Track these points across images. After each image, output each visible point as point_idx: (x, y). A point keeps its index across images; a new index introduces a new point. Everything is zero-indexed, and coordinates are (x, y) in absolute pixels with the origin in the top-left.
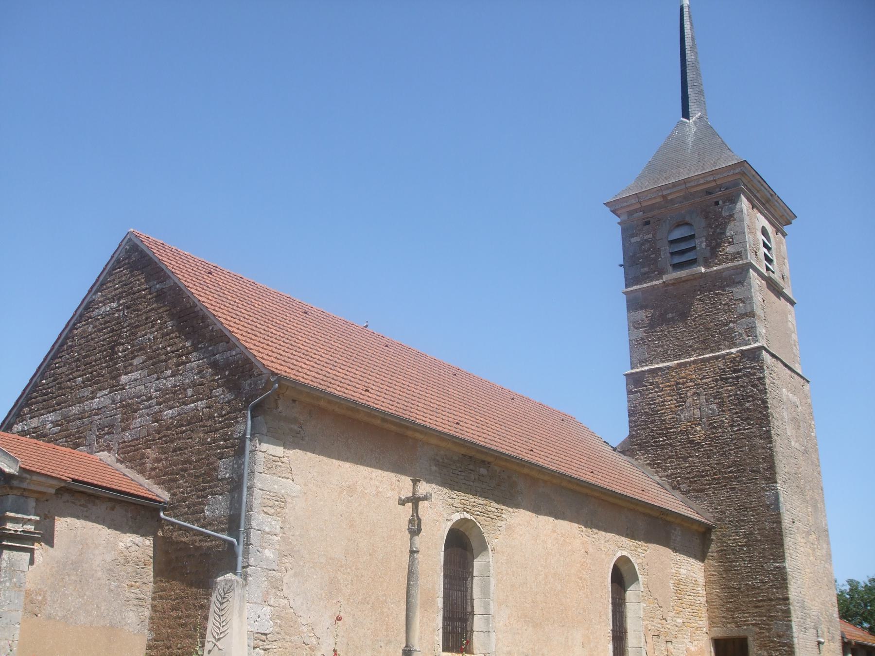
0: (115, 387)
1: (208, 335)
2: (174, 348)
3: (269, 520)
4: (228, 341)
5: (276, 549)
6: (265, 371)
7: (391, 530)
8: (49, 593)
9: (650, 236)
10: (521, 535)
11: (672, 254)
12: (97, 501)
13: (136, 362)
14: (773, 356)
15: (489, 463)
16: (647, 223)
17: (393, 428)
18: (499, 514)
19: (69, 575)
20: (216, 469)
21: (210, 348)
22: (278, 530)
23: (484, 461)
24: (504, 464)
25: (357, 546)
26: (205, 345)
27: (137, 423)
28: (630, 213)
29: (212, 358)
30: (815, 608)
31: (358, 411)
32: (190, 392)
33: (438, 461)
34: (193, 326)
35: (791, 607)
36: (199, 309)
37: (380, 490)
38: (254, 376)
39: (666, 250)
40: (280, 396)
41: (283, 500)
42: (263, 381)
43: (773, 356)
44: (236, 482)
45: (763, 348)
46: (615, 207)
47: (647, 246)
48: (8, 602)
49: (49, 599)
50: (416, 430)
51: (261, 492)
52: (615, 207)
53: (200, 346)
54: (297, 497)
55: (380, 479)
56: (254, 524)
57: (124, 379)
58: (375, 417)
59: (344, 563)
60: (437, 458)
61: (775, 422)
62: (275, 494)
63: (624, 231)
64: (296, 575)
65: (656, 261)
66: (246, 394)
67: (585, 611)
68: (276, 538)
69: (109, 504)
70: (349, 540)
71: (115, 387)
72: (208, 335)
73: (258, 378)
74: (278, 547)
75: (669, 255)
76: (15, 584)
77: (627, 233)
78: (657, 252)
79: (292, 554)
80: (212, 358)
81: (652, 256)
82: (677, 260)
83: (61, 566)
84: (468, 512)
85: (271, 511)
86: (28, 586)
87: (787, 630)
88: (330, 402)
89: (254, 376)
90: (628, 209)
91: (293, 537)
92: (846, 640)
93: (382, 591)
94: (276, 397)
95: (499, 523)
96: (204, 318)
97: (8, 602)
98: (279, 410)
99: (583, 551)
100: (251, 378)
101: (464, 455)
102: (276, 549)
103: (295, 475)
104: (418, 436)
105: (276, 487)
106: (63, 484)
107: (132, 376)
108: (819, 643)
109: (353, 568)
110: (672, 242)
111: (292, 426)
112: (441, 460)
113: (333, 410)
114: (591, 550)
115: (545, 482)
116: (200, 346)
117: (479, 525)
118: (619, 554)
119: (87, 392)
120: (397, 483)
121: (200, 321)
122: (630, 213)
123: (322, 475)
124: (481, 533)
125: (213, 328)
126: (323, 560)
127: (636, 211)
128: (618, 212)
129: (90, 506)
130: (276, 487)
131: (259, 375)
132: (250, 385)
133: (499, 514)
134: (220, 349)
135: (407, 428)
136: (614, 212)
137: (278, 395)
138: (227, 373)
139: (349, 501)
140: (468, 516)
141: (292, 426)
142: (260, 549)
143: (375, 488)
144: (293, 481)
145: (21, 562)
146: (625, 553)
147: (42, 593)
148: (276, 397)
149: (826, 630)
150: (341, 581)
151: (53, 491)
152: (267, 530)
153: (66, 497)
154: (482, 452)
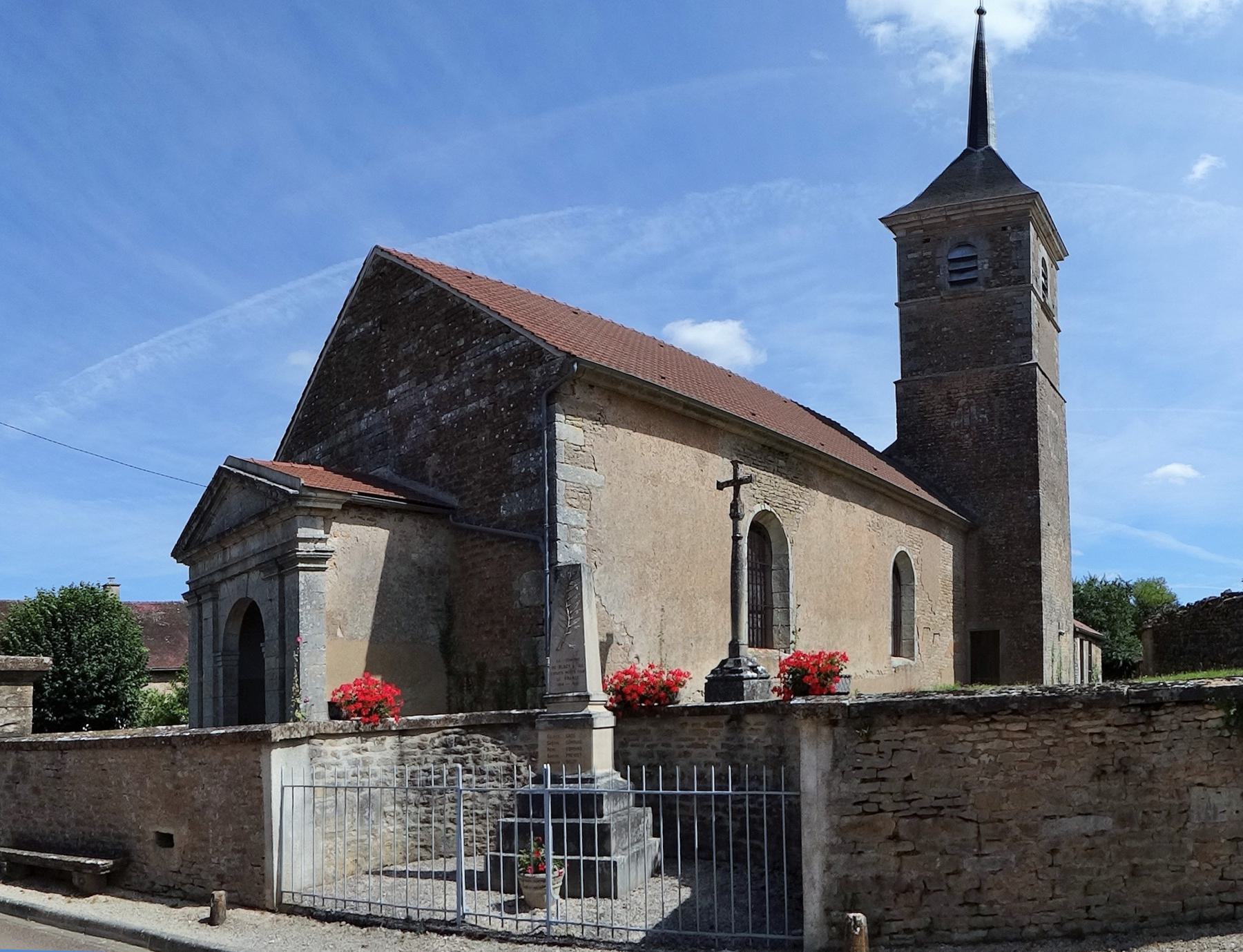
0: (382, 403)
1: (482, 330)
2: (445, 351)
3: (576, 512)
4: (507, 330)
5: (584, 544)
6: (558, 355)
7: (696, 522)
8: (349, 613)
9: (930, 253)
10: (816, 528)
11: (951, 272)
12: (385, 513)
13: (402, 374)
14: (1043, 373)
15: (787, 454)
16: (927, 241)
17: (696, 415)
18: (797, 507)
19: (366, 592)
20: (510, 465)
21: (487, 343)
22: (585, 524)
23: (782, 453)
24: (801, 455)
25: (664, 538)
26: (480, 340)
27: (412, 434)
28: (909, 230)
29: (491, 352)
30: (1058, 602)
31: (659, 396)
32: (468, 392)
33: (739, 451)
34: (464, 324)
35: (1043, 602)
36: (468, 305)
37: (684, 479)
38: (546, 362)
39: (945, 267)
40: (577, 382)
41: (587, 491)
42: (558, 364)
43: (1043, 373)
44: (534, 476)
45: (1036, 364)
46: (890, 221)
47: (925, 262)
48: (311, 625)
49: (350, 618)
50: (717, 418)
51: (564, 483)
52: (890, 221)
53: (474, 342)
54: (601, 487)
55: (685, 468)
56: (559, 518)
57: (391, 393)
58: (677, 403)
59: (652, 556)
60: (739, 448)
61: (1041, 435)
62: (578, 486)
63: (899, 247)
64: (605, 571)
65: (934, 277)
66: (537, 382)
67: (871, 604)
68: (583, 532)
69: (398, 516)
70: (656, 532)
71: (382, 403)
72: (482, 330)
73: (551, 363)
74: (585, 541)
75: (947, 272)
76: (315, 606)
77: (903, 249)
78: (937, 269)
79: (601, 549)
80: (491, 352)
81: (930, 272)
82: (956, 278)
83: (357, 584)
84: (768, 504)
85: (575, 503)
86: (328, 607)
87: (1038, 622)
88: (630, 386)
89: (546, 362)
90: (906, 226)
91: (600, 531)
92: (1077, 630)
93: (690, 585)
94: (572, 383)
95: (798, 516)
96: (476, 313)
97: (311, 625)
98: (576, 396)
99: (870, 545)
100: (541, 364)
101: (764, 446)
102: (584, 544)
103: (598, 464)
104: (720, 424)
105: (579, 477)
106: (348, 498)
107: (400, 389)
108: (1060, 634)
109: (662, 562)
110: (951, 261)
111: (591, 413)
112: (742, 450)
113: (633, 395)
114: (877, 545)
115: (838, 475)
116: (474, 342)
117: (778, 516)
118: (899, 550)
119: (352, 415)
120: (701, 473)
121: (471, 317)
122: (909, 230)
123: (626, 464)
124: (780, 525)
125: (488, 322)
126: (632, 554)
127: (915, 228)
128: (894, 228)
129: (377, 519)
130: (579, 477)
131: (551, 360)
132: (541, 372)
133: (797, 507)
134: (500, 341)
135: (709, 415)
136: (890, 228)
137: (574, 380)
138: (511, 364)
139: (654, 491)
140: (768, 508)
141: (591, 413)
142: (568, 546)
143: (679, 477)
144: (596, 470)
145: (318, 583)
146: (904, 549)
147: (342, 613)
148: (572, 383)
149: (1065, 623)
150: (651, 575)
151: (339, 507)
152: (574, 523)
153: (353, 512)
154: (781, 442)
